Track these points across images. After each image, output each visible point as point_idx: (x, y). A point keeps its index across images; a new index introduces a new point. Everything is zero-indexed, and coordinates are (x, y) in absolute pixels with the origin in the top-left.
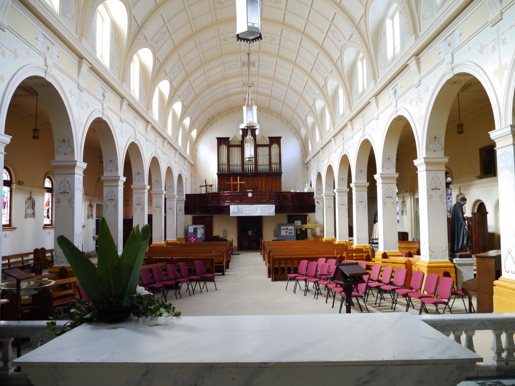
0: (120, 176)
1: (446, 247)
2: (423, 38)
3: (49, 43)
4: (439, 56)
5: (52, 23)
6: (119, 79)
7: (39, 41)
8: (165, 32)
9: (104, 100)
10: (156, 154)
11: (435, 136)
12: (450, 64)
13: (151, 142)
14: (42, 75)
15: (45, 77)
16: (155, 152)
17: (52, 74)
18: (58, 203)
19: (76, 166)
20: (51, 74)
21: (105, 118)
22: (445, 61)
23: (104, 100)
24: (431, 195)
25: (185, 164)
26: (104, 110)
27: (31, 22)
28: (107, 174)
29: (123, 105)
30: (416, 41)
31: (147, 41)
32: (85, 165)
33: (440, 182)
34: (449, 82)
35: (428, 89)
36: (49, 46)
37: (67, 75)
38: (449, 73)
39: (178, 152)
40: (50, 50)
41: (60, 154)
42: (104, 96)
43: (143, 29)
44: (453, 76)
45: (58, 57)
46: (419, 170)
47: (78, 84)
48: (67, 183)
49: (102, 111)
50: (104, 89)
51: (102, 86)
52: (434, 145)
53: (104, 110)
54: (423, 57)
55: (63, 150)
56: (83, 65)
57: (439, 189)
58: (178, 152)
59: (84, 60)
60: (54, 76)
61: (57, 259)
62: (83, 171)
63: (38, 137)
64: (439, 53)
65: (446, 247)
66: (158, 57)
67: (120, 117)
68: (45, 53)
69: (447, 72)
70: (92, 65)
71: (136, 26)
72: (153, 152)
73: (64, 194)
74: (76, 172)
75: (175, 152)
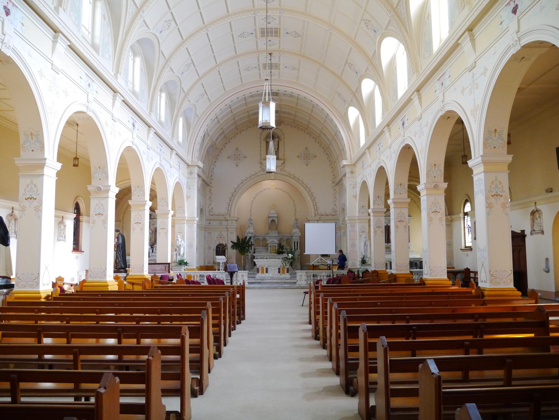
0: (147, 201)
1: (511, 270)
2: (470, 16)
3: (90, 81)
4: (435, 93)
5: (47, 14)
6: (113, 71)
7: (20, 22)
8: (170, 20)
9: (134, 129)
10: (179, 179)
11: (496, 129)
12: (516, 34)
13: (154, 150)
14: (84, 109)
15: (87, 111)
16: (179, 177)
17: (11, 46)
18: (93, 224)
19: (109, 190)
20: (9, 46)
21: (134, 147)
22: (509, 30)
23: (134, 129)
24: (24, 206)
25: (171, 157)
26: (133, 139)
27: (41, 29)
28: (95, 182)
29: (116, 100)
30: (470, 11)
31: (173, 73)
32: (59, 166)
33: (502, 187)
34: (514, 58)
35: (486, 69)
36: (90, 83)
37: (82, 89)
38: (514, 46)
39: (152, 131)
40: (91, 86)
41: (27, 151)
42: (134, 126)
43: (169, 62)
44: (520, 48)
45: (97, 92)
46: (475, 172)
47: (112, 115)
48: (140, 217)
49: (86, 104)
50: (134, 119)
51: (133, 117)
52: (434, 172)
53: (133, 139)
54: (423, 92)
55: (137, 193)
56: (59, 40)
57: (501, 195)
58: (152, 131)
59: (60, 34)
60: (94, 111)
61: (92, 274)
62: (56, 172)
63: (78, 165)
64: (500, 23)
65: (511, 270)
66: (183, 88)
67: (112, 115)
68: (86, 89)
69: (511, 45)
70: (72, 42)
71: (134, 8)
72: (156, 162)
73: (30, 200)
74: (45, 173)
75: (148, 130)
